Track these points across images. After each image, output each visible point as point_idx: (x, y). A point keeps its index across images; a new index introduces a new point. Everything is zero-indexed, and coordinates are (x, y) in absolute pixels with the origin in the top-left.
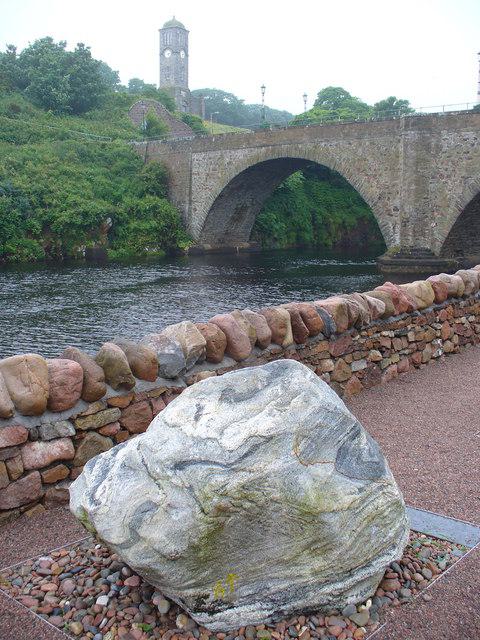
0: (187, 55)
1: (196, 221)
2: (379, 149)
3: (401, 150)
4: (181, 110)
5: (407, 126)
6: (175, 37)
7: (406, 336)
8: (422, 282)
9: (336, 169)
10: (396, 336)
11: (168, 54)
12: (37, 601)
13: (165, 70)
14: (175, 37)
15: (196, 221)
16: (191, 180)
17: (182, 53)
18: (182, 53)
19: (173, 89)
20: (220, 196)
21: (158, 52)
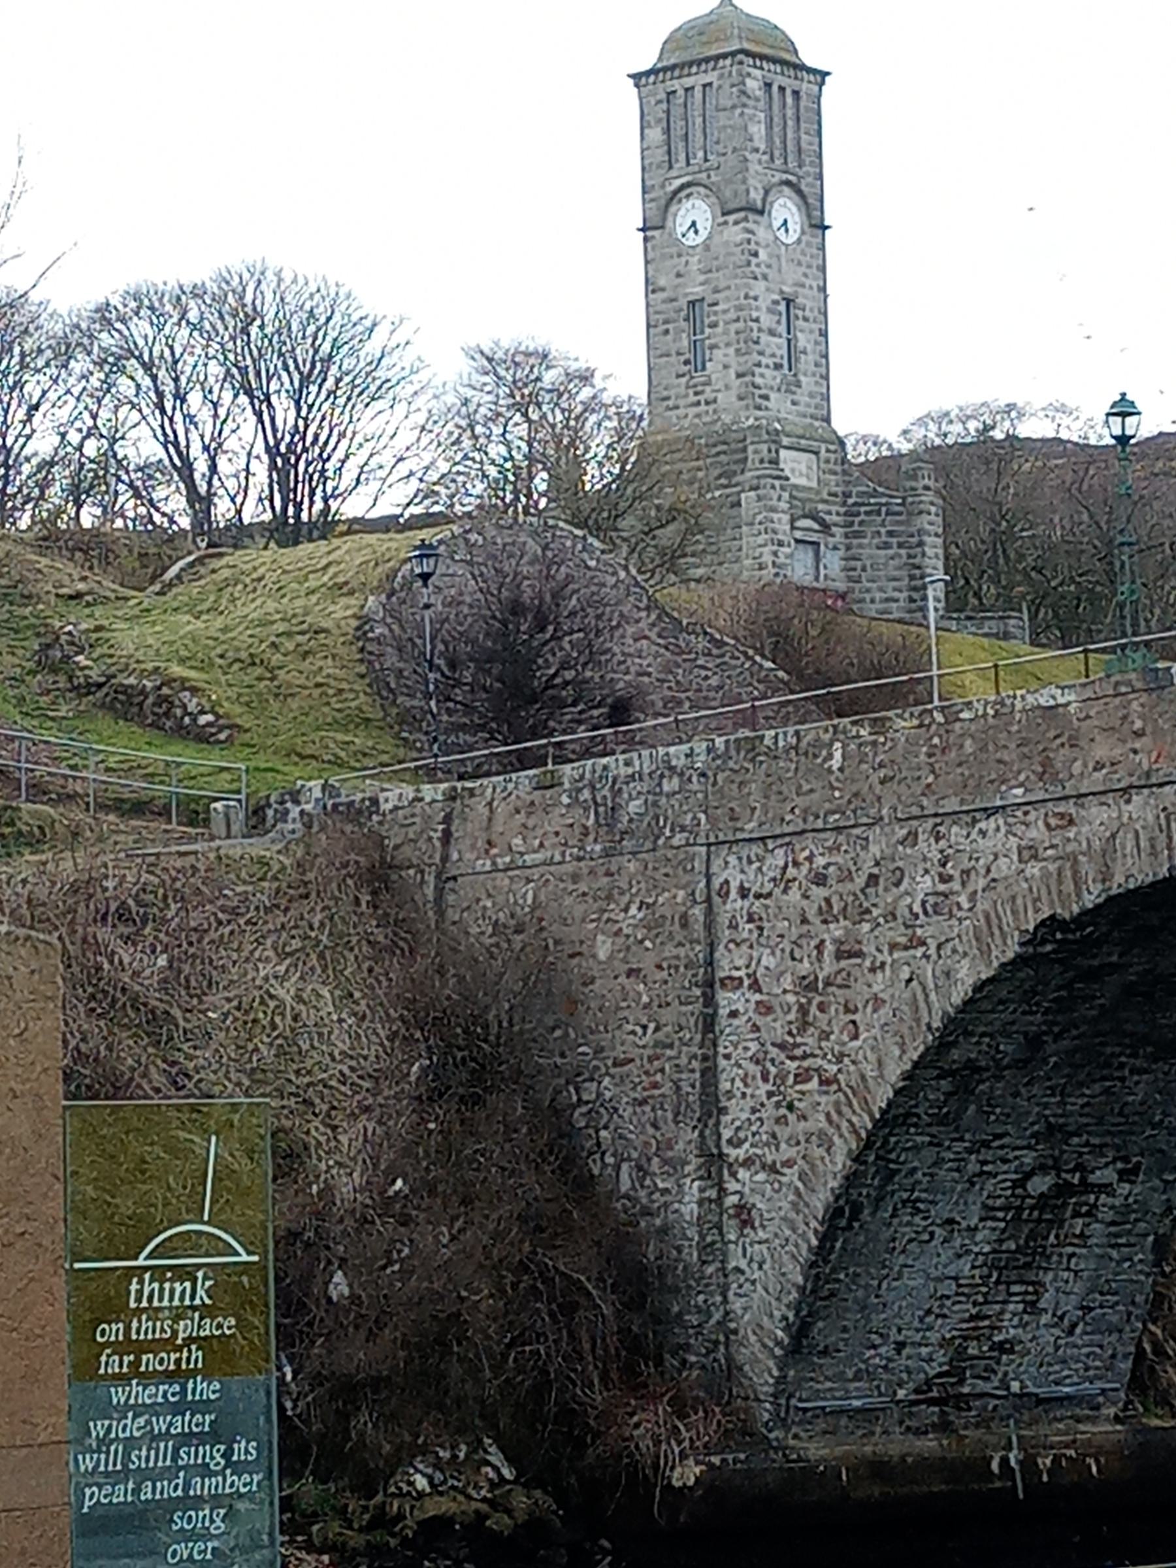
0: (653, 226)
4: (768, 551)
6: (732, 121)
11: (695, 215)
13: (680, 322)
14: (732, 121)
16: (709, 1023)
17: (785, 209)
20: (890, 1120)
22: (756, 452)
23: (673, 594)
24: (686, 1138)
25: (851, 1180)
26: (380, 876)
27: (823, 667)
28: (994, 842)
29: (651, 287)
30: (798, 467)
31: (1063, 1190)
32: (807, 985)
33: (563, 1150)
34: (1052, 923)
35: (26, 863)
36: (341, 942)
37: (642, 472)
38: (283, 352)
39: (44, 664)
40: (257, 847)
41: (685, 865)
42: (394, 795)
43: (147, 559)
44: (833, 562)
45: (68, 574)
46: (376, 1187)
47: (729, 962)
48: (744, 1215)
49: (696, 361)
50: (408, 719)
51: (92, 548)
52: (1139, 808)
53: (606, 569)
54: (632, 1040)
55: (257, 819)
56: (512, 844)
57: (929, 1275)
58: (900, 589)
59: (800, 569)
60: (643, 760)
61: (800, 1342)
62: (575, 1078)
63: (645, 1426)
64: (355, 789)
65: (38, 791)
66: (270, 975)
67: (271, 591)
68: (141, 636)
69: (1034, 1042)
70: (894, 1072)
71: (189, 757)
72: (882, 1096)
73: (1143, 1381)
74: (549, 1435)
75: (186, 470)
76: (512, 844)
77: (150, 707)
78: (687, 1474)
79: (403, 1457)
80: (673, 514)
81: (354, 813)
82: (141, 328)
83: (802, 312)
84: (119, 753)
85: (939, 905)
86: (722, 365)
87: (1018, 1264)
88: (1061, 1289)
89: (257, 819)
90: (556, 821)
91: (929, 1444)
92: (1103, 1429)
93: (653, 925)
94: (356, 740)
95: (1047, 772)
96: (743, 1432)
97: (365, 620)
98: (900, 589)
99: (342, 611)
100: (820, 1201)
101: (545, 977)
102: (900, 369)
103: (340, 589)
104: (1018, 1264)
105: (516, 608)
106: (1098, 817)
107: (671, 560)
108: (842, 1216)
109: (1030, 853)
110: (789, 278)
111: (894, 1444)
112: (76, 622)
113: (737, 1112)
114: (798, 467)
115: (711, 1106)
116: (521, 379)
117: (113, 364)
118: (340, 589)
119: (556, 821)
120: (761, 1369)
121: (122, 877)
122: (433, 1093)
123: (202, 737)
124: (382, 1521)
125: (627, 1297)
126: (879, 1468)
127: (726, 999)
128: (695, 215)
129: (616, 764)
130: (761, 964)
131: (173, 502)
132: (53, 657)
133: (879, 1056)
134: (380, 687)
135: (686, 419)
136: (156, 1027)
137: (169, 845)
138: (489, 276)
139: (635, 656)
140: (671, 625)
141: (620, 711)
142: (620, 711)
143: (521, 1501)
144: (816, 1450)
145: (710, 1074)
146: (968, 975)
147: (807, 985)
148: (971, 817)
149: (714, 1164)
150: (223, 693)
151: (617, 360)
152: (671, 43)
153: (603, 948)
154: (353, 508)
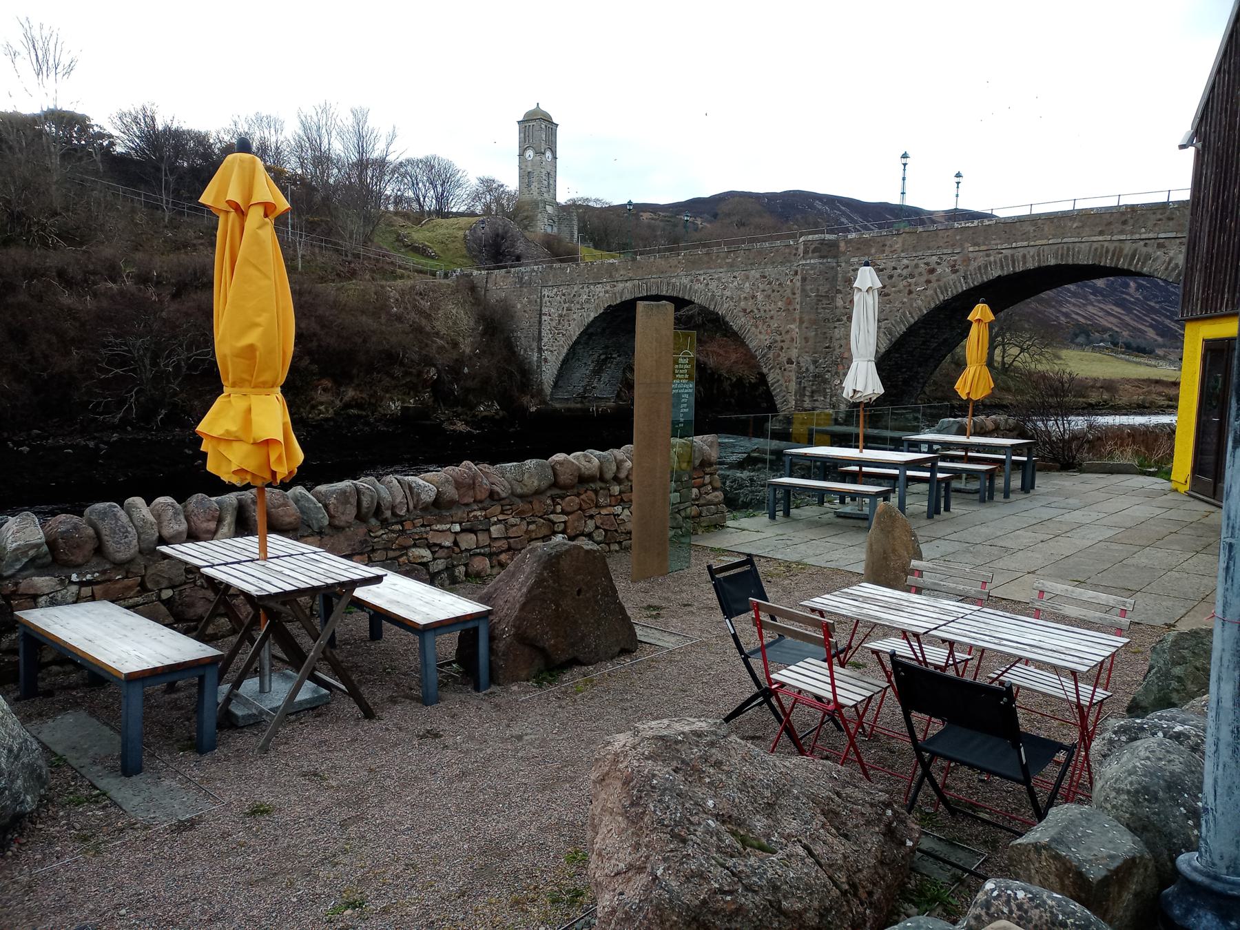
0: (521, 155)
1: (548, 374)
2: (770, 283)
3: (798, 284)
4: (543, 226)
5: (806, 252)
6: (538, 131)
7: (489, 530)
8: (615, 451)
9: (717, 310)
10: (463, 531)
11: (530, 154)
12: (750, 689)
13: (526, 176)
14: (538, 131)
15: (548, 374)
16: (540, 322)
17: (548, 154)
18: (548, 154)
19: (535, 204)
20: (576, 343)
21: (516, 150)
22: (541, 205)
23: (527, 234)
24: (535, 345)
25: (567, 354)
26: (473, 288)
27: (558, 252)
28: (599, 288)
29: (520, 168)
30: (549, 209)
31: (607, 358)
32: (560, 316)
33: (510, 345)
34: (610, 306)
35: (399, 282)
36: (465, 301)
37: (519, 208)
38: (439, 176)
39: (397, 240)
40: (447, 281)
41: (536, 290)
42: (475, 273)
43: (420, 217)
44: (555, 229)
45: (400, 221)
46: (473, 351)
47: (545, 310)
48: (546, 360)
49: (529, 185)
50: (475, 256)
51: (405, 216)
52: (629, 284)
53: (515, 228)
54: (525, 324)
55: (446, 276)
56: (499, 284)
57: (581, 373)
58: (571, 235)
59: (549, 230)
60: (528, 269)
61: (556, 385)
62: (512, 331)
63: (525, 400)
64: (467, 271)
65: (400, 267)
66: (451, 308)
67: (444, 227)
68: (419, 235)
69: (604, 330)
70: (577, 334)
71: (431, 262)
72: (574, 338)
73: (618, 396)
74: (507, 400)
75: (418, 200)
76: (499, 284)
77: (420, 251)
78: (533, 409)
79: (479, 403)
80: (527, 217)
81: (467, 276)
82: (409, 168)
83: (551, 176)
84: (414, 260)
85: (588, 301)
86: (535, 186)
87: (597, 372)
88: (605, 377)
89: (446, 276)
90: (510, 280)
91: (579, 405)
92: (611, 404)
93: (530, 302)
94: (300, 254)
95: (611, 276)
96: (544, 402)
97: (465, 236)
98: (571, 235)
99: (461, 233)
100: (561, 358)
101: (507, 311)
102: (569, 188)
103: (460, 229)
104: (597, 372)
105: (497, 235)
106: (621, 285)
107: (526, 228)
108: (565, 362)
109: (606, 292)
110: (549, 168)
111: (573, 405)
112: (403, 232)
113: (545, 340)
114: (549, 209)
115: (540, 339)
116: (489, 185)
117: (404, 175)
118: (460, 229)
119: (510, 280)
120: (548, 390)
121: (420, 287)
122: (484, 333)
123: (432, 258)
124: (474, 416)
125: (524, 375)
126: (569, 410)
127: (544, 318)
128: (530, 154)
129: (522, 269)
130: (551, 312)
131: (415, 206)
132: (399, 239)
133: (574, 330)
134: (468, 249)
135: (527, 197)
136: (428, 317)
137: (430, 279)
138: (486, 161)
139: (520, 247)
140: (527, 241)
141: (518, 258)
142: (518, 258)
143: (501, 413)
144: (557, 406)
145: (540, 332)
146: (593, 315)
147: (560, 316)
148: (595, 284)
149: (540, 350)
150: (436, 249)
151: (511, 181)
152: (527, 114)
153: (519, 306)
154: (454, 210)
